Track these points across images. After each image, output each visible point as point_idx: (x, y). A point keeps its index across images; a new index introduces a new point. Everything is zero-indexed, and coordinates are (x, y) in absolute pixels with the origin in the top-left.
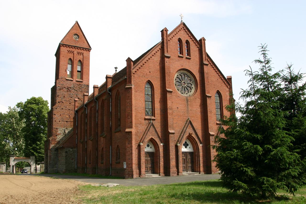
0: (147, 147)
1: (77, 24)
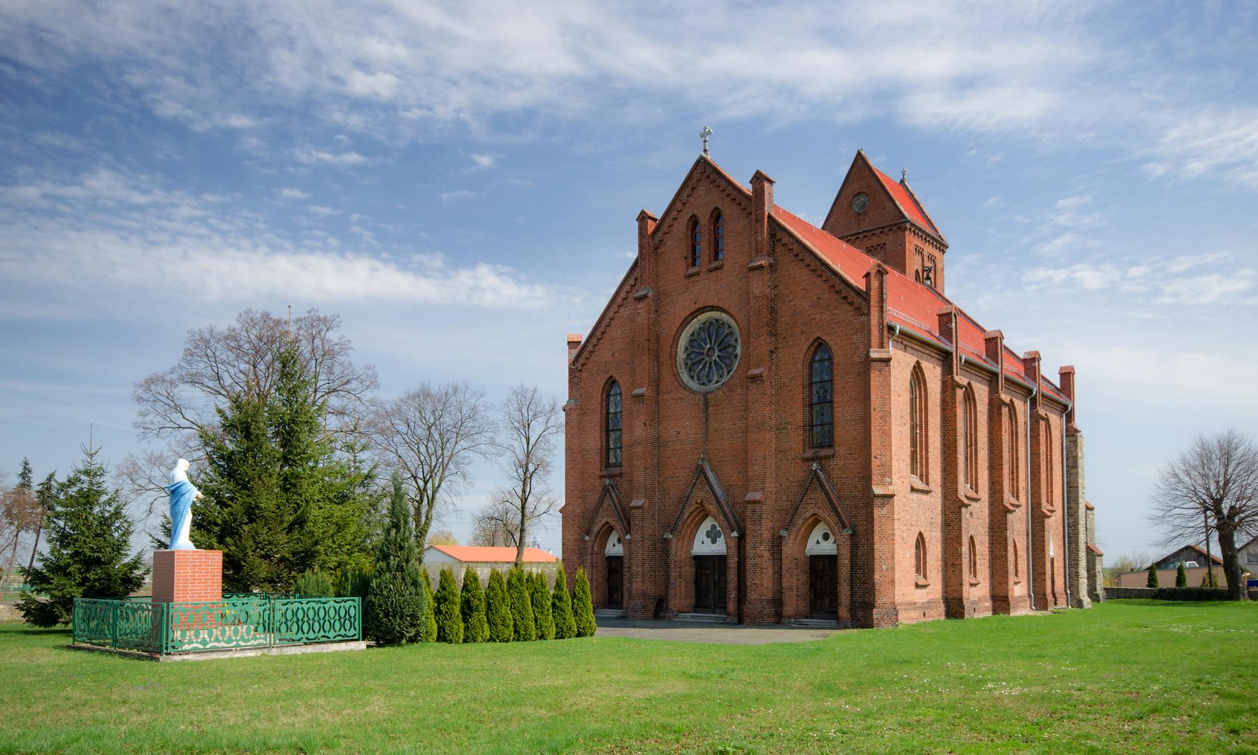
0: (821, 540)
1: (860, 163)
